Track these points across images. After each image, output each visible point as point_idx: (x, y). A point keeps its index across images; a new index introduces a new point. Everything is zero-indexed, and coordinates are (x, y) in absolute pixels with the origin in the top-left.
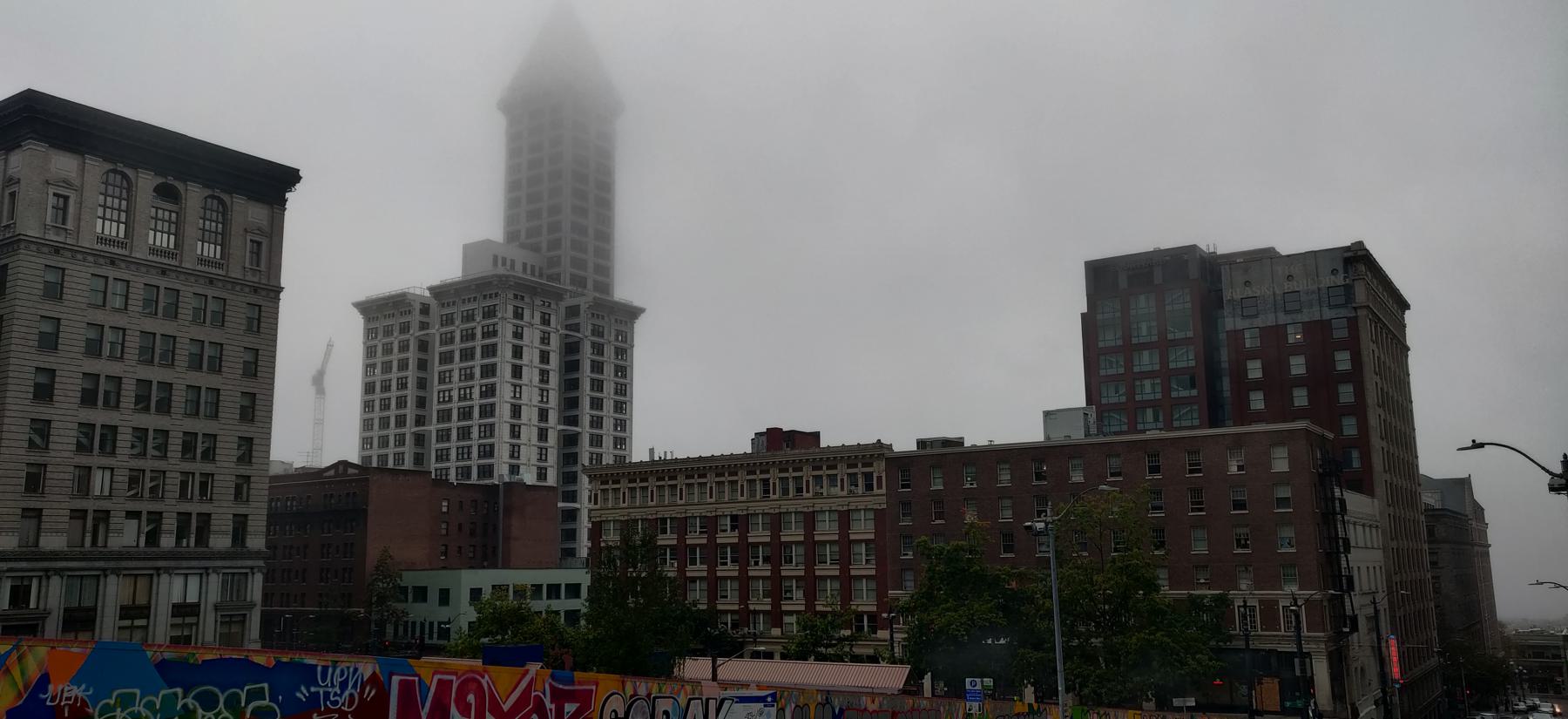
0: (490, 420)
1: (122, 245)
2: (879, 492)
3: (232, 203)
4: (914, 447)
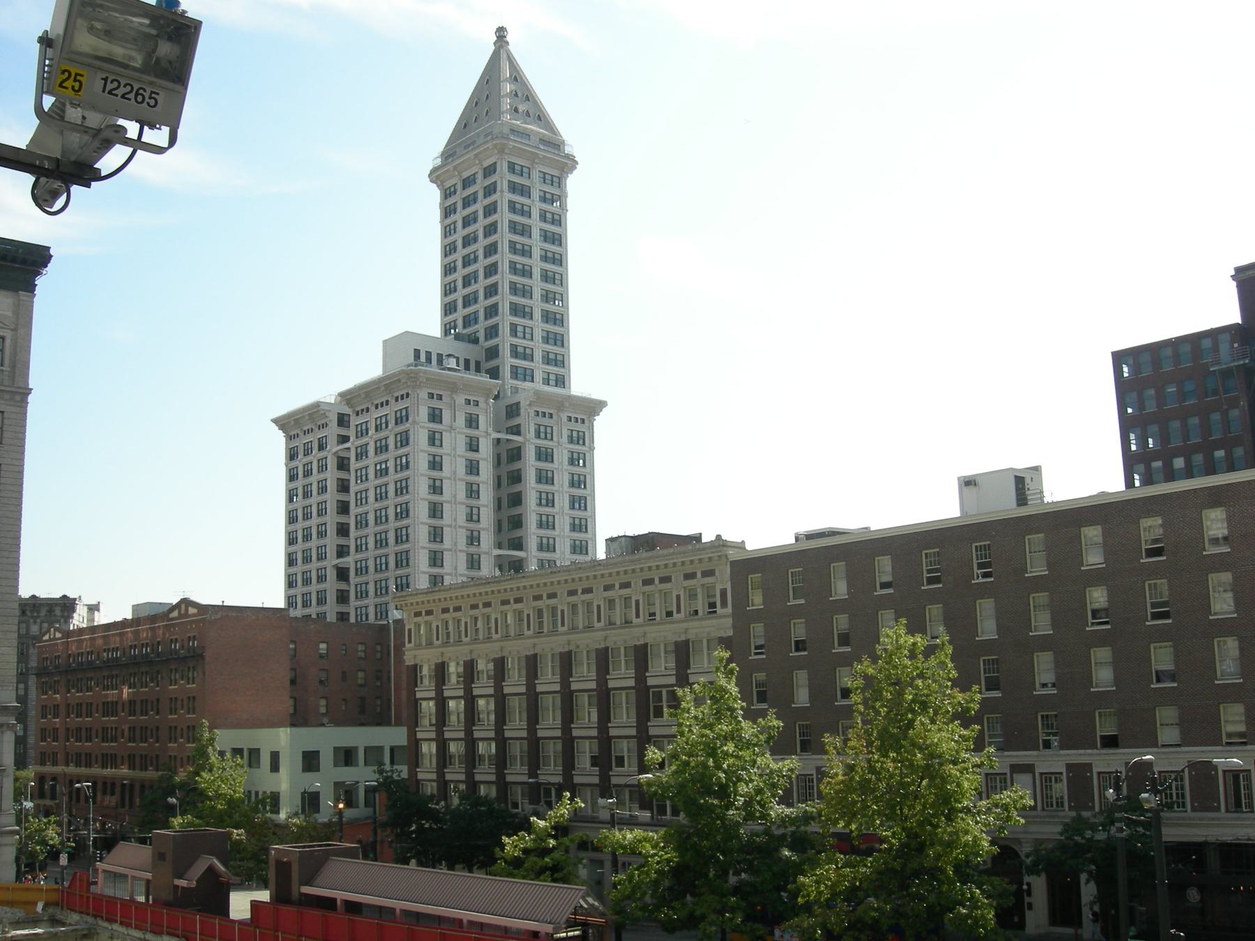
0: (405, 546)
4: (793, 541)
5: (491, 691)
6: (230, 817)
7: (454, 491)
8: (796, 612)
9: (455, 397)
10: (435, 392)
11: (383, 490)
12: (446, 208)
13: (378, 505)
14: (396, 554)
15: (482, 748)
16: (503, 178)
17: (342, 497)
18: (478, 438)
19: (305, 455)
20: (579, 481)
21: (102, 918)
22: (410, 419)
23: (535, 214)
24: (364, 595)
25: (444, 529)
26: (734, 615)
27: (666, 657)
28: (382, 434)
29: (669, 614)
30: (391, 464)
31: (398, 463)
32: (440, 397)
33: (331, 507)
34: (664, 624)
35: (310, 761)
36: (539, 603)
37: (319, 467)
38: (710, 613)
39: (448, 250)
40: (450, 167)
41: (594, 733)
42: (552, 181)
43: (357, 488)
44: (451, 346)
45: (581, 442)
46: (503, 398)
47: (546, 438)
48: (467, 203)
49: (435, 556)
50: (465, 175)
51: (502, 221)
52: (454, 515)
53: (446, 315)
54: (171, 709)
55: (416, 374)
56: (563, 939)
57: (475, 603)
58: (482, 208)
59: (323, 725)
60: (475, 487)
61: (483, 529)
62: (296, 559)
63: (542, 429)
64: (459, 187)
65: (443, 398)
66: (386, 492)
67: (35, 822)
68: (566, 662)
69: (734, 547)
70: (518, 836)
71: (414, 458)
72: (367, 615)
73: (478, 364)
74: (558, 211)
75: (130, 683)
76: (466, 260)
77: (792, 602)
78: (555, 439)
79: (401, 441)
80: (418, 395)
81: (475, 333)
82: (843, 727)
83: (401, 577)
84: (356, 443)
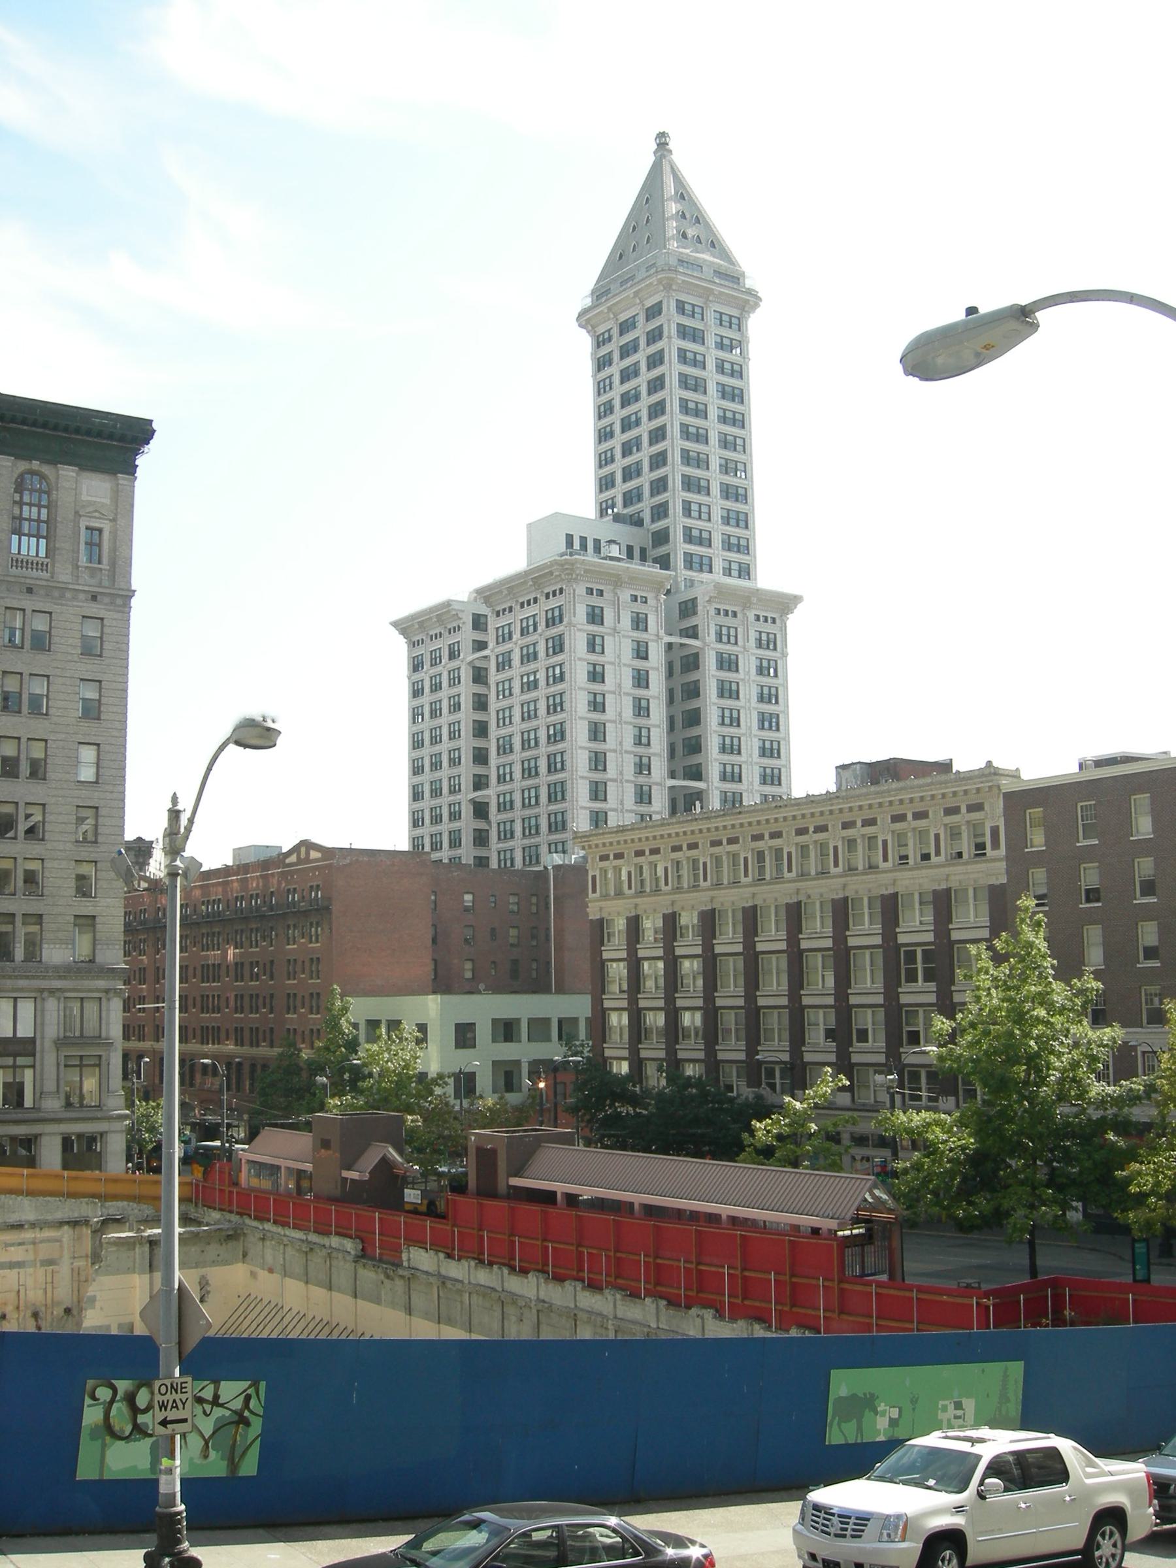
0: (560, 776)
1: (42, 567)
2: (996, 853)
3: (58, 478)
4: (1077, 770)
5: (699, 951)
6: (398, 1097)
7: (619, 708)
8: (1087, 854)
9: (618, 592)
10: (595, 587)
11: (532, 708)
12: (599, 359)
13: (525, 726)
14: (549, 785)
15: (687, 1019)
16: (671, 320)
17: (480, 716)
18: (647, 643)
19: (432, 665)
20: (770, 695)
21: (250, 1216)
22: (566, 620)
23: (711, 364)
24: (508, 836)
25: (608, 754)
26: (1007, 858)
27: (921, 910)
28: (529, 639)
29: (926, 857)
30: (541, 676)
31: (551, 673)
32: (601, 593)
33: (466, 729)
34: (918, 869)
35: (464, 1035)
36: (760, 845)
37: (450, 679)
38: (977, 855)
39: (604, 410)
40: (603, 308)
41: (830, 1001)
42: (731, 323)
43: (499, 704)
44: (607, 530)
45: (771, 646)
46: (676, 593)
47: (729, 642)
48: (625, 352)
49: (597, 787)
50: (623, 317)
51: (671, 373)
52: (619, 738)
53: (601, 491)
54: (289, 973)
55: (573, 564)
56: (847, 1237)
57: (677, 844)
58: (645, 359)
59: (479, 992)
60: (643, 703)
61: (655, 755)
62: (423, 792)
63: (724, 631)
64: (615, 332)
65: (604, 594)
66: (536, 710)
67: (142, 1106)
68: (751, 919)
69: (1007, 776)
70: (772, 1119)
71: (571, 669)
72: (512, 860)
73: (643, 551)
74: (739, 360)
75: (236, 942)
76: (626, 422)
77: (1082, 843)
78: (740, 642)
79: (554, 647)
80: (574, 590)
81: (638, 513)
82: (1146, 995)
83: (555, 814)
84: (496, 650)
